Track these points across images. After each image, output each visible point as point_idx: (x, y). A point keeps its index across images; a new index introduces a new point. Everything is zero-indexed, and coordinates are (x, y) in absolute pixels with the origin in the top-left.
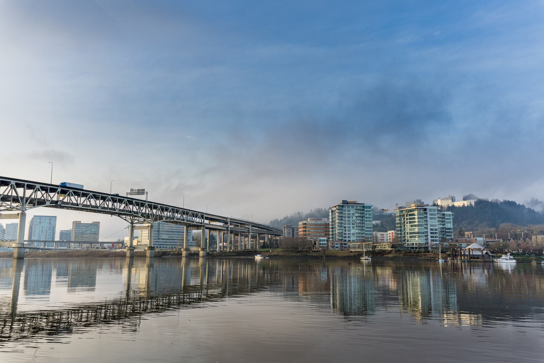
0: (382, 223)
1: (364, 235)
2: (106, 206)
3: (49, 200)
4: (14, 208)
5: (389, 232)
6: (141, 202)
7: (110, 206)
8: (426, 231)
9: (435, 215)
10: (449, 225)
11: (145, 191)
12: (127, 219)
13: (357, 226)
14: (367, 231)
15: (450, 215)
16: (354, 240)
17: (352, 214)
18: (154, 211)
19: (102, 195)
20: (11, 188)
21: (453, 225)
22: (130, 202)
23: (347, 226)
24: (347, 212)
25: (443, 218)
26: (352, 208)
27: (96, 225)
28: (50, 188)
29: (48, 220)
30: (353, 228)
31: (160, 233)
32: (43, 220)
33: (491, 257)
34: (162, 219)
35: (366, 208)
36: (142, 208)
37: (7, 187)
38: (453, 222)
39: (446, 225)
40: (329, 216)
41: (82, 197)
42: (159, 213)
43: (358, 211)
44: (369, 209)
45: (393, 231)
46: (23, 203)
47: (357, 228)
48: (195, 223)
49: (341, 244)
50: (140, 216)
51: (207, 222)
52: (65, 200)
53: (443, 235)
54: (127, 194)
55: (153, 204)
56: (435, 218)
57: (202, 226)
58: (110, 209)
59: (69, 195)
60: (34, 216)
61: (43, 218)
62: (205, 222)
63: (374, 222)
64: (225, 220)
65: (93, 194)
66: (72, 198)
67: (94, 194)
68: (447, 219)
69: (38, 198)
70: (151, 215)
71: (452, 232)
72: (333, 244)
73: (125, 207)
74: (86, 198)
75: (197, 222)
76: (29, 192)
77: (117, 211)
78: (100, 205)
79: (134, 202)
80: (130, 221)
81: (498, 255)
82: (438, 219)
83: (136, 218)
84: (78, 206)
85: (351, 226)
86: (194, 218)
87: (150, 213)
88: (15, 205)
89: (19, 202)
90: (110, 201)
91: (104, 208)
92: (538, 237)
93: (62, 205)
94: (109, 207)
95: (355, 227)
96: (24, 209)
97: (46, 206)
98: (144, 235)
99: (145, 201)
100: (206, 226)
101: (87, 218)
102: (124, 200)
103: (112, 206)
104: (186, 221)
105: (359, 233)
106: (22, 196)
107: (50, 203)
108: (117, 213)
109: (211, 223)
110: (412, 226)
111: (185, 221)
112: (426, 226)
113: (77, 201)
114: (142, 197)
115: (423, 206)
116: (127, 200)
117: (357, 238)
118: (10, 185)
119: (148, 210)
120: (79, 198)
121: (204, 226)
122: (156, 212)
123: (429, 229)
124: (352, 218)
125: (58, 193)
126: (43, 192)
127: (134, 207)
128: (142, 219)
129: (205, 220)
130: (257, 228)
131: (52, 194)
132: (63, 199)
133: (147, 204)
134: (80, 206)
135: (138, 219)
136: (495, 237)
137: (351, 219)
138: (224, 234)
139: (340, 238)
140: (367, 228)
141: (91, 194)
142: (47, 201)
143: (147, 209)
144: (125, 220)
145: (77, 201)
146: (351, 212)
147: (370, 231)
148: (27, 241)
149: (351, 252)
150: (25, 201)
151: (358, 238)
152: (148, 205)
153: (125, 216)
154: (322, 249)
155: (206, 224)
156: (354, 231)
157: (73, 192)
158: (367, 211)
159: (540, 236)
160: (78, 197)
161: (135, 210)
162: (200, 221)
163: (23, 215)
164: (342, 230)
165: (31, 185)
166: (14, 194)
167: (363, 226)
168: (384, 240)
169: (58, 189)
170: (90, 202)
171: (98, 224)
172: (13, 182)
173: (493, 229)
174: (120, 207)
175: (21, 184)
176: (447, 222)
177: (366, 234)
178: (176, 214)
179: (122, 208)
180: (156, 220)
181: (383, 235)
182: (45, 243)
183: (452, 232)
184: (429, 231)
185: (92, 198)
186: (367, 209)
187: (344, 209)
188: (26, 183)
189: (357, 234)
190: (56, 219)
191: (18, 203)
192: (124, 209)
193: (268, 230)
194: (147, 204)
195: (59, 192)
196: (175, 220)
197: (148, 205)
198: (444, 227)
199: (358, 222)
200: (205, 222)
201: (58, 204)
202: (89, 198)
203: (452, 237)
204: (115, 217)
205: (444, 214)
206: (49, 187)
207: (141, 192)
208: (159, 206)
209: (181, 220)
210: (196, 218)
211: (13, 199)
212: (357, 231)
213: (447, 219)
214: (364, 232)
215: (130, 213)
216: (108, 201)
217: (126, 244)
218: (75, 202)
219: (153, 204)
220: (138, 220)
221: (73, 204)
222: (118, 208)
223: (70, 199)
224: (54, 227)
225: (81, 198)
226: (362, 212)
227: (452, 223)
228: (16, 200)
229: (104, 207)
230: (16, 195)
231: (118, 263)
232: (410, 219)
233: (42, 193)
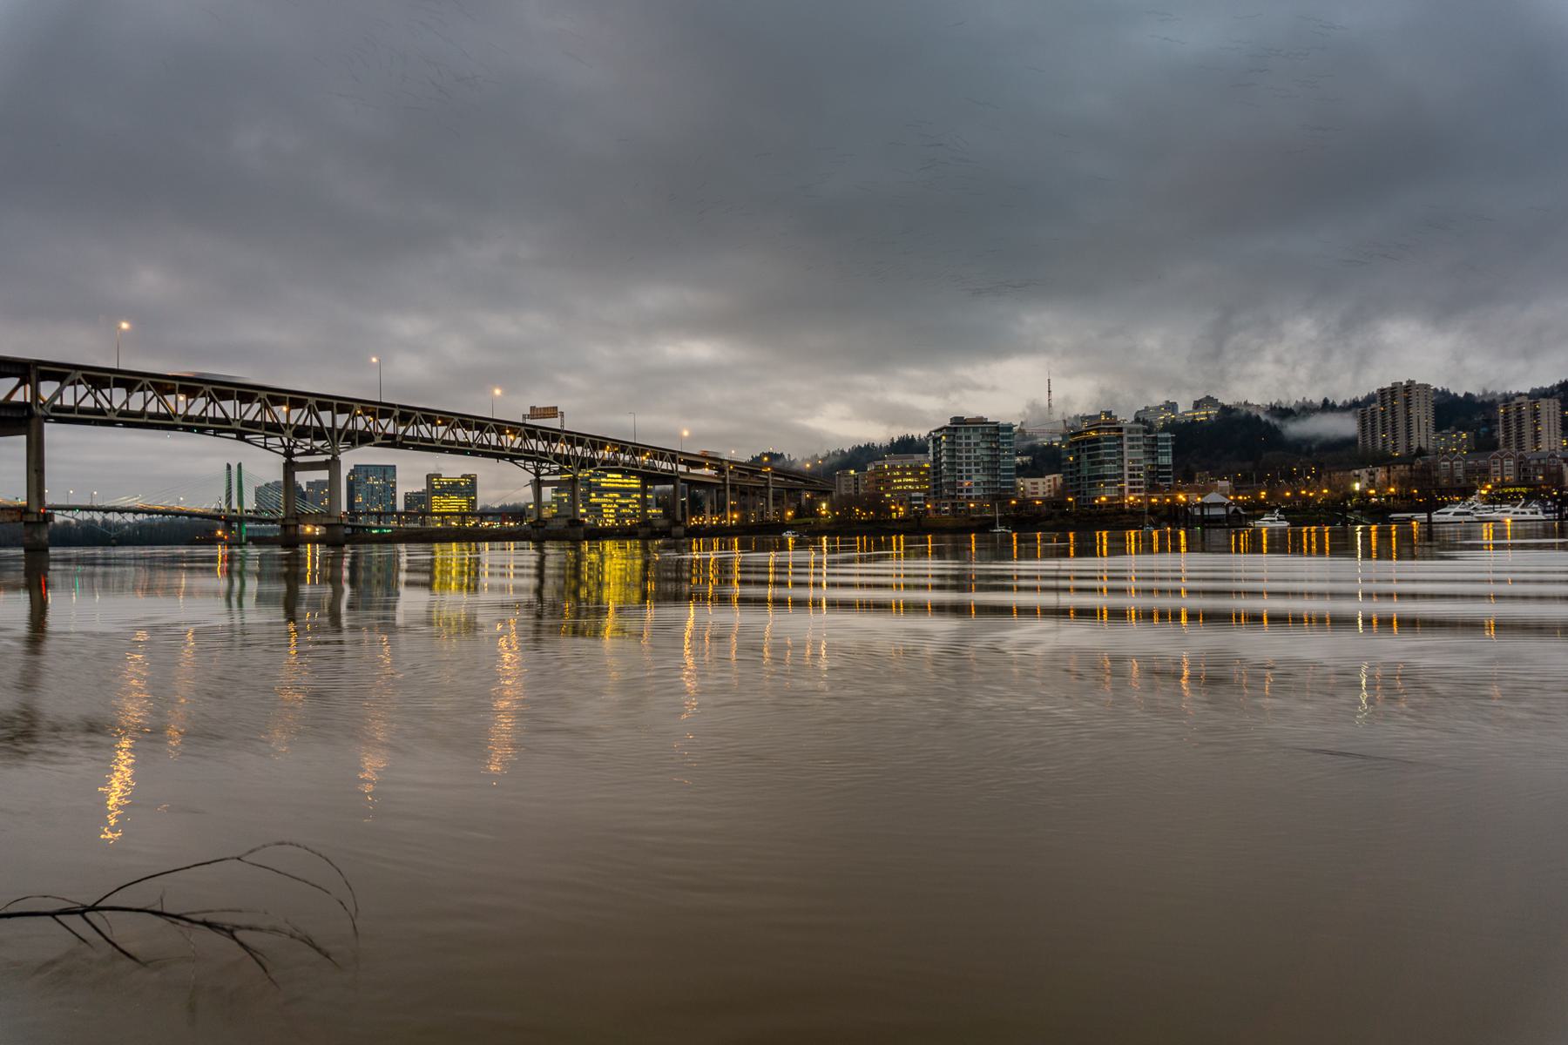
0: (1033, 462)
1: (998, 486)
2: (485, 442)
3: (338, 430)
4: (317, 449)
5: (1048, 477)
6: (291, 396)
7: (494, 443)
8: (1120, 472)
9: (1138, 439)
10: (1166, 460)
11: (559, 410)
12: (527, 467)
13: (984, 469)
14: (1004, 477)
15: (1166, 440)
16: (979, 496)
17: (974, 443)
18: (579, 449)
19: (340, 402)
20: (309, 412)
21: (1174, 459)
22: (531, 432)
23: (964, 468)
24: (964, 441)
25: (1153, 446)
26: (973, 430)
27: (388, 472)
28: (238, 392)
30: (977, 471)
33: (1244, 519)
34: (596, 466)
35: (1003, 431)
36: (554, 445)
37: (249, 405)
38: (1174, 452)
39: (1159, 460)
40: (928, 449)
41: (114, 387)
42: (589, 454)
43: (986, 439)
44: (1008, 434)
45: (1056, 476)
46: (332, 440)
47: (984, 471)
48: (659, 472)
49: (953, 504)
51: (682, 468)
52: (410, 433)
53: (1154, 479)
54: (524, 417)
55: (575, 436)
56: (1138, 446)
58: (494, 447)
59: (415, 423)
62: (679, 470)
63: (1018, 459)
64: (719, 463)
66: (422, 428)
67: (424, 413)
68: (1162, 447)
69: (358, 429)
70: (573, 457)
71: (1169, 473)
72: (936, 505)
73: (521, 444)
74: (348, 415)
75: (663, 470)
76: (342, 420)
77: (508, 452)
78: (474, 441)
80: (533, 471)
81: (1257, 512)
82: (1143, 447)
83: (544, 465)
84: (434, 443)
85: (973, 467)
86: (656, 462)
87: (570, 453)
88: (318, 444)
89: (325, 438)
90: (493, 431)
91: (482, 446)
92: (1332, 475)
93: (405, 442)
94: (492, 444)
95: (981, 471)
96: (336, 452)
97: (375, 445)
99: (559, 431)
100: (682, 477)
101: (453, 467)
102: (414, 414)
105: (988, 482)
106: (331, 426)
107: (383, 439)
108: (507, 456)
109: (691, 471)
110: (1093, 463)
111: (640, 469)
112: (1119, 463)
113: (431, 434)
114: (553, 423)
115: (1115, 424)
116: (268, 396)
117: (984, 491)
118: (307, 405)
120: (434, 428)
121: (677, 477)
122: (583, 453)
123: (1126, 469)
124: (975, 452)
125: (395, 420)
126: (369, 418)
127: (540, 443)
128: (556, 467)
129: (679, 466)
130: (783, 479)
131: (383, 422)
132: (405, 431)
133: (563, 436)
134: (438, 444)
135: (548, 466)
136: (1252, 479)
137: (972, 454)
138: (718, 492)
139: (952, 493)
140: (1004, 470)
141: (456, 419)
142: (286, 428)
144: (524, 468)
145: (431, 434)
146: (972, 441)
147: (1010, 477)
149: (973, 519)
150: (335, 436)
151: (987, 493)
152: (566, 437)
153: (523, 461)
154: (915, 516)
155: (682, 473)
156: (979, 477)
157: (422, 415)
158: (1003, 437)
159: (1337, 474)
160: (432, 426)
161: (541, 448)
162: (670, 468)
163: (333, 465)
164: (955, 476)
165: (344, 405)
166: (316, 423)
167: (997, 466)
168: (1037, 493)
169: (393, 411)
170: (455, 434)
172: (312, 401)
173: (1249, 464)
174: (512, 442)
175: (326, 403)
176: (1162, 454)
177: (1004, 484)
178: (622, 455)
179: (516, 445)
181: (1036, 483)
182: (379, 517)
183: (1169, 473)
184: (1126, 472)
185: (459, 427)
186: (1004, 434)
187: (958, 434)
188: (335, 402)
189: (984, 485)
190: (395, 471)
191: (324, 439)
193: (805, 481)
194: (563, 436)
195: (395, 417)
196: (620, 466)
197: (566, 437)
198: (1156, 463)
199: (986, 459)
200: (679, 470)
201: (397, 439)
202: (453, 427)
203: (1171, 483)
204: (505, 465)
205: (1155, 439)
206: (378, 407)
207: (552, 412)
208: (588, 439)
209: (633, 466)
210: (660, 462)
211: (359, 437)
212: (985, 479)
213: (1162, 447)
214: (998, 479)
215: (530, 456)
216: (488, 432)
218: (427, 435)
219: (575, 436)
220: (549, 468)
221: (423, 439)
222: (509, 445)
223: (418, 430)
224: (394, 490)
225: (114, 390)
226: (993, 439)
227: (1171, 454)
228: (319, 434)
229: (449, 441)
230: (224, 417)
232: (1089, 449)
233: (365, 421)
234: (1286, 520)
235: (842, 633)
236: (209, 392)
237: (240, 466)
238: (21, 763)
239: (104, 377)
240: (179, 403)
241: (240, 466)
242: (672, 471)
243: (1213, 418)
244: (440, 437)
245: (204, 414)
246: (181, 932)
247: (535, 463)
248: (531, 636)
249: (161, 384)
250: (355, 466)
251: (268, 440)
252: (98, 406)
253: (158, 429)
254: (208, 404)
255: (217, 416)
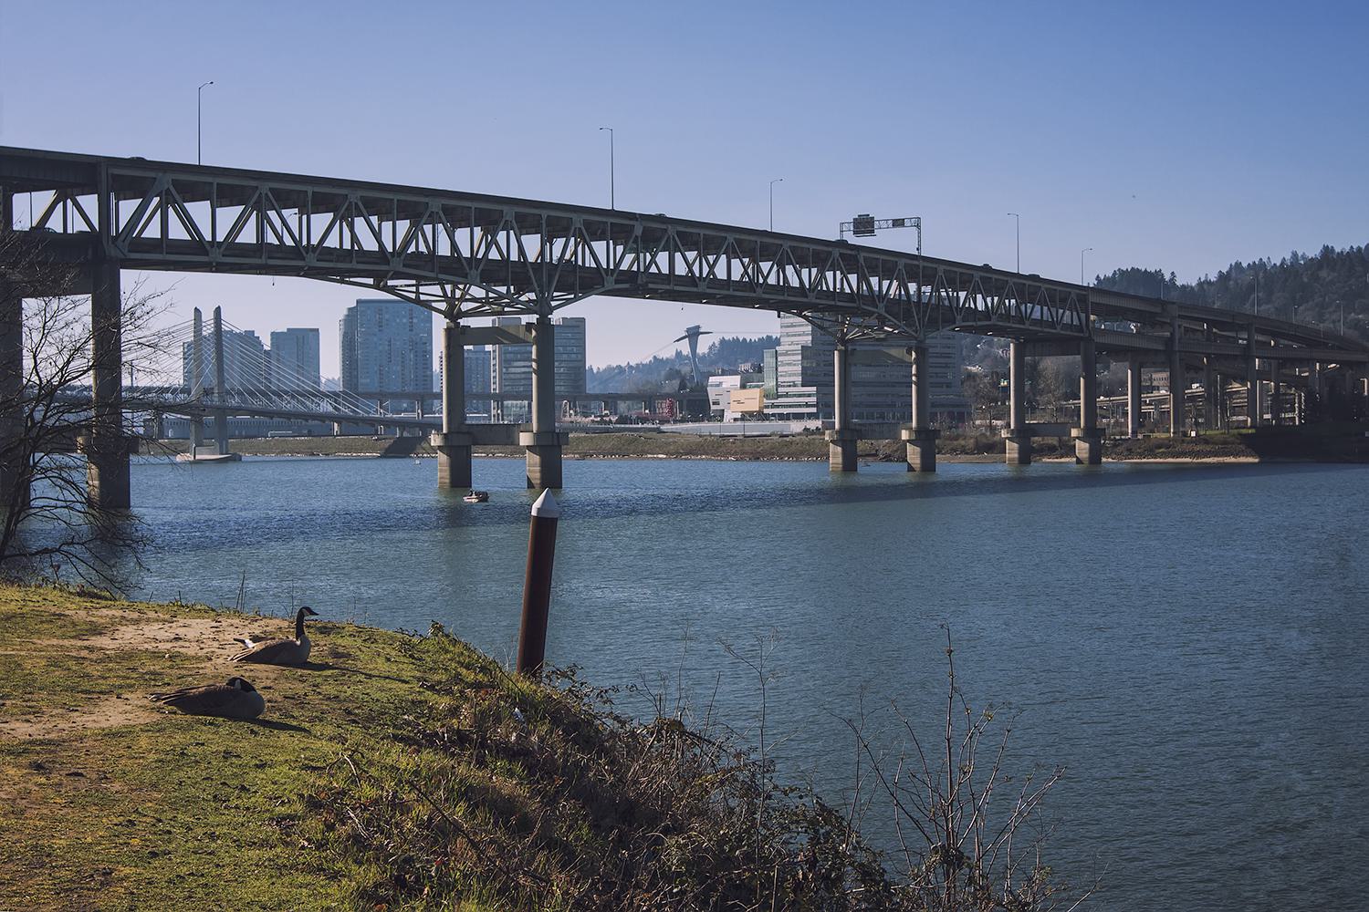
19: (553, 213)
29: (404, 317)
31: (782, 362)
32: (387, 316)
50: (882, 311)
57: (1081, 338)
60: (358, 302)
61: (387, 308)
65: (735, 239)
67: (681, 229)
79: (862, 261)
98: (786, 368)
103: (380, 226)
104: (1062, 329)
119: (827, 283)
143: (678, 255)
148: (334, 396)
160: (381, 221)
171: (578, 327)
180: (933, 324)
192: (635, 268)
217: (714, 403)
231: (323, 480)
233: (743, 264)
236: (356, 204)
237: (218, 311)
239: (196, 183)
241: (218, 311)
242: (1052, 325)
243: (418, 446)
244: (315, 241)
247: (448, 288)
249: (454, 208)
251: (422, 289)
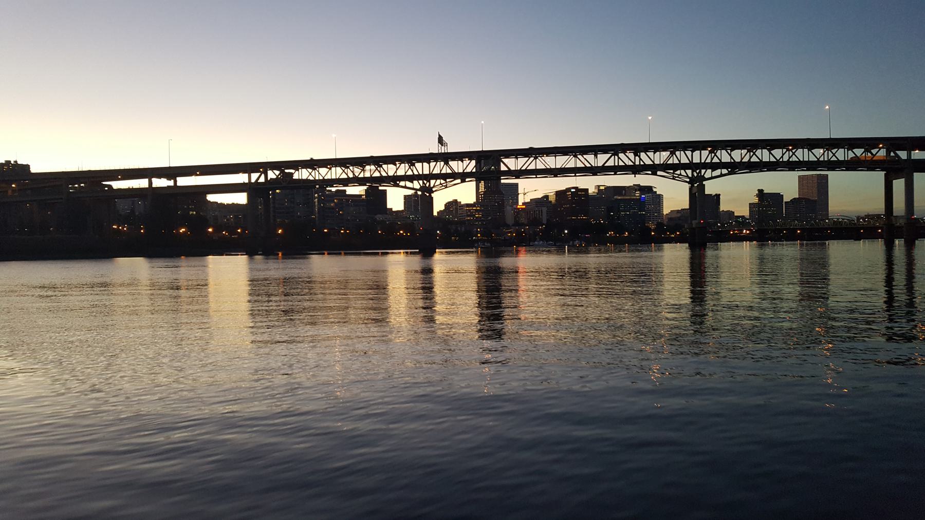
94: (636, 164)
160: (636, 155)
234: (663, 163)
235: (58, 429)
238: (176, 264)
240: (764, 155)
245: (781, 160)
246: (907, 367)
248: (420, 303)
250: (783, 195)
252: (732, 161)
253: (556, 176)
254: (824, 152)
255: (620, 164)
